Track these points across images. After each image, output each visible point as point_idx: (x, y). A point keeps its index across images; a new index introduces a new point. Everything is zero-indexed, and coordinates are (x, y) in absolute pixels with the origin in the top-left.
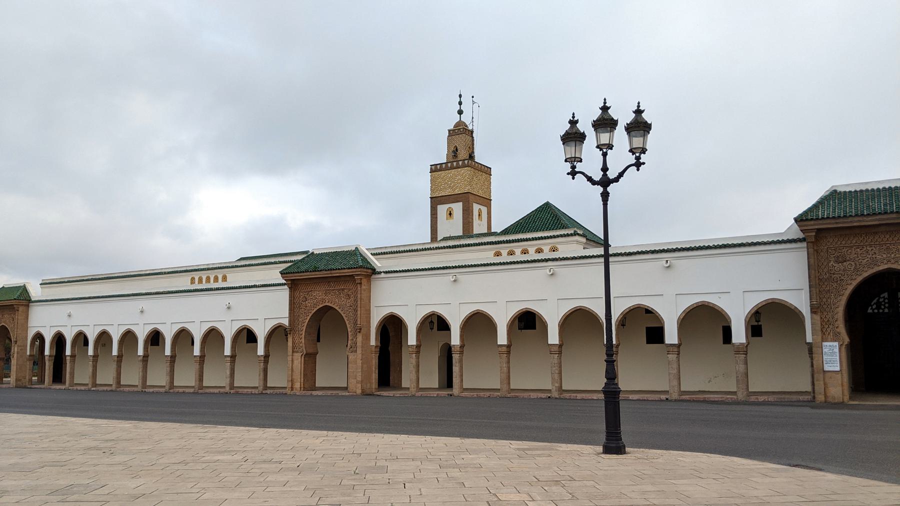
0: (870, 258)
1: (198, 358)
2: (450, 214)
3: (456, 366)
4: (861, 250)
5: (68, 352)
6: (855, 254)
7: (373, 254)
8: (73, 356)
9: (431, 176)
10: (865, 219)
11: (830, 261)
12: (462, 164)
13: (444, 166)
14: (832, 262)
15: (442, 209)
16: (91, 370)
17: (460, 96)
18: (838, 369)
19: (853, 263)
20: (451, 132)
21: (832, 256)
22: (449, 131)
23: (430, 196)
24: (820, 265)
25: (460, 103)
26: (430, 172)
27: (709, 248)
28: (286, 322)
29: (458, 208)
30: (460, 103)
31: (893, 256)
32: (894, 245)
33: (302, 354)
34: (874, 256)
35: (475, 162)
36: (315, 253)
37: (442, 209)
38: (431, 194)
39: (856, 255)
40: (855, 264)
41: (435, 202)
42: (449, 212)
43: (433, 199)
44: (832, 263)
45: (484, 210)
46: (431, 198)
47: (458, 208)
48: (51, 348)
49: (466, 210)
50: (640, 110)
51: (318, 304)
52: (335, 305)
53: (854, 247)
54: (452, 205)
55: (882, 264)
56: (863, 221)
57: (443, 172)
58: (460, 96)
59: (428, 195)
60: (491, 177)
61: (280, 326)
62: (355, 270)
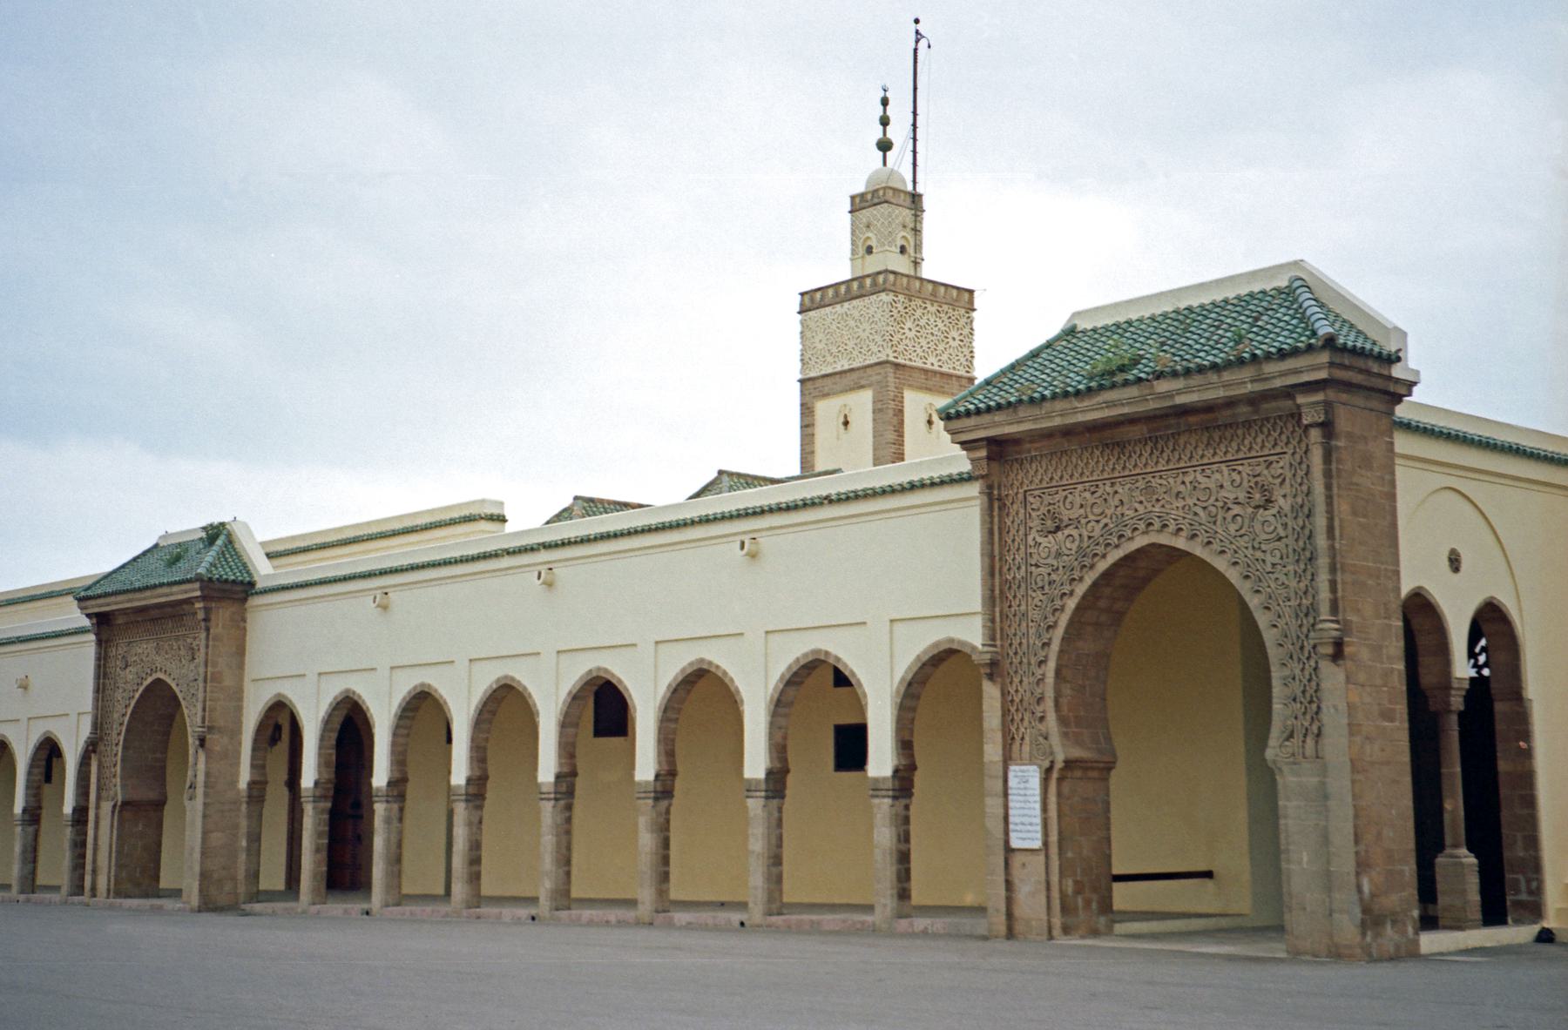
0: (1111, 518)
2: (846, 423)
3: (1348, 873)
4: (1093, 493)
5: (380, 776)
6: (1082, 506)
8: (398, 784)
9: (802, 323)
10: (1077, 404)
11: (1031, 528)
12: (871, 286)
13: (831, 292)
14: (1034, 531)
15: (827, 409)
16: (647, 840)
18: (1037, 844)
19: (1075, 533)
20: (857, 200)
21: (1034, 514)
22: (853, 198)
23: (799, 376)
26: (799, 313)
28: (972, 634)
29: (861, 403)
32: (1161, 477)
35: (921, 279)
37: (827, 409)
38: (801, 373)
39: (1082, 511)
40: (1080, 535)
41: (812, 388)
43: (809, 385)
44: (1033, 534)
46: (802, 382)
47: (861, 403)
48: (323, 763)
53: (1080, 487)
56: (1075, 411)
57: (828, 309)
59: (794, 372)
60: (974, 314)
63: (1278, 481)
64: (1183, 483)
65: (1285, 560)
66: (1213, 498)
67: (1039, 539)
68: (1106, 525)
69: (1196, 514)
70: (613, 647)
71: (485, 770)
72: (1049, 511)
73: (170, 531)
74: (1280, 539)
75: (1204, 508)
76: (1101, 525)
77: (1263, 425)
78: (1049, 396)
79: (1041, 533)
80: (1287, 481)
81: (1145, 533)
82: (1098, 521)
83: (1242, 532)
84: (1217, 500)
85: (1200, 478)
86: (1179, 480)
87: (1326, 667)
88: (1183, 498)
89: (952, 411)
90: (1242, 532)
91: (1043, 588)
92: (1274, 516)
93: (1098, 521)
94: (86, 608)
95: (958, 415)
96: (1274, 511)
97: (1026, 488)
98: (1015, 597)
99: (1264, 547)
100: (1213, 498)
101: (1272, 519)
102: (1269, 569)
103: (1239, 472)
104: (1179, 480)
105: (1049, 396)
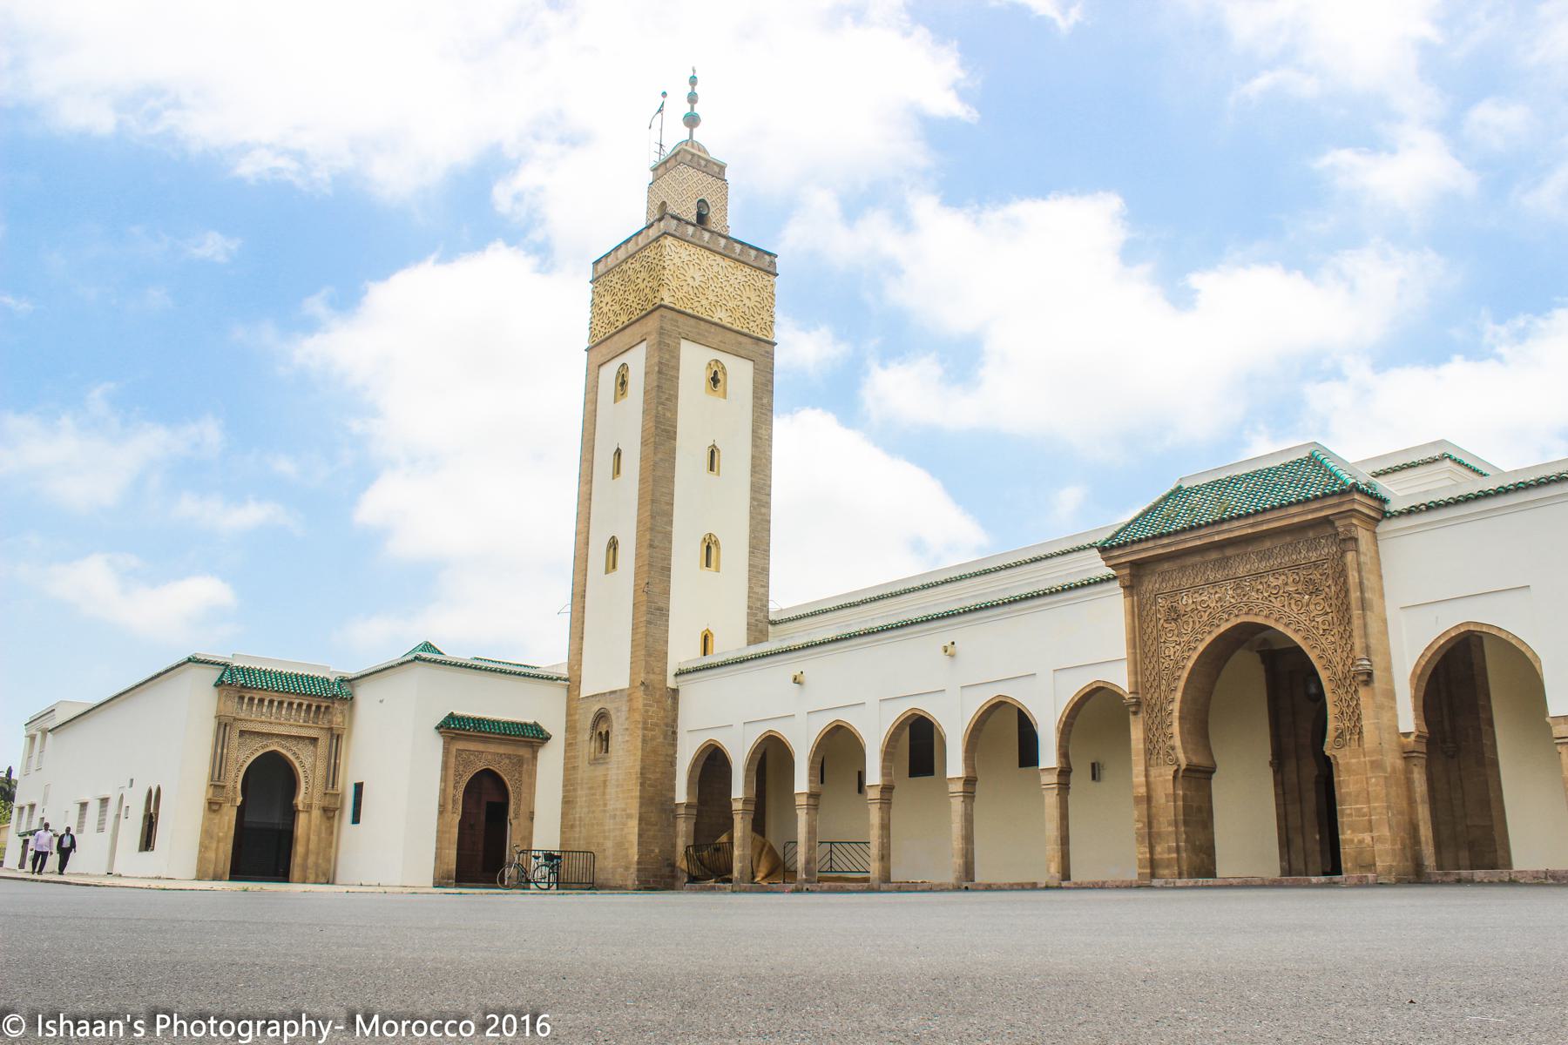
1: (805, 796)
7: (1389, 485)
17: (693, 81)
24: (1145, 638)
25: (692, 99)
27: (1526, 487)
28: (1121, 679)
30: (692, 99)
31: (1244, 599)
32: (1245, 581)
33: (1175, 767)
34: (1219, 605)
36: (1185, 486)
42: (620, 381)
45: (740, 372)
49: (769, 381)
50: (962, 65)
51: (1216, 621)
52: (1293, 627)
54: (729, 361)
55: (1185, 661)
58: (693, 81)
61: (1103, 688)
62: (1172, 539)
63: (1324, 577)
64: (1261, 583)
65: (1331, 626)
66: (1281, 591)
67: (1166, 625)
68: (1211, 613)
69: (1270, 601)
70: (89, 711)
71: (1068, 763)
72: (1172, 606)
73: (784, 608)
74: (1327, 613)
75: (1276, 598)
76: (1207, 614)
77: (1172, 573)
78: (207, 855)
79: (442, 730)
80: (1330, 576)
81: (1247, 614)
82: (1205, 612)
83: (1302, 611)
84: (1284, 592)
85: (1271, 579)
86: (1258, 582)
87: (1362, 691)
88: (1262, 593)
89: (1107, 545)
90: (1302, 611)
91: (1170, 656)
92: (1323, 599)
93: (1205, 612)
94: (1111, 558)
95: (1112, 547)
96: (1322, 597)
97: (1155, 593)
98: (1150, 662)
99: (1317, 619)
100: (1281, 591)
101: (1322, 601)
102: (1321, 632)
103: (1298, 574)
104: (1258, 582)
105: (207, 855)
